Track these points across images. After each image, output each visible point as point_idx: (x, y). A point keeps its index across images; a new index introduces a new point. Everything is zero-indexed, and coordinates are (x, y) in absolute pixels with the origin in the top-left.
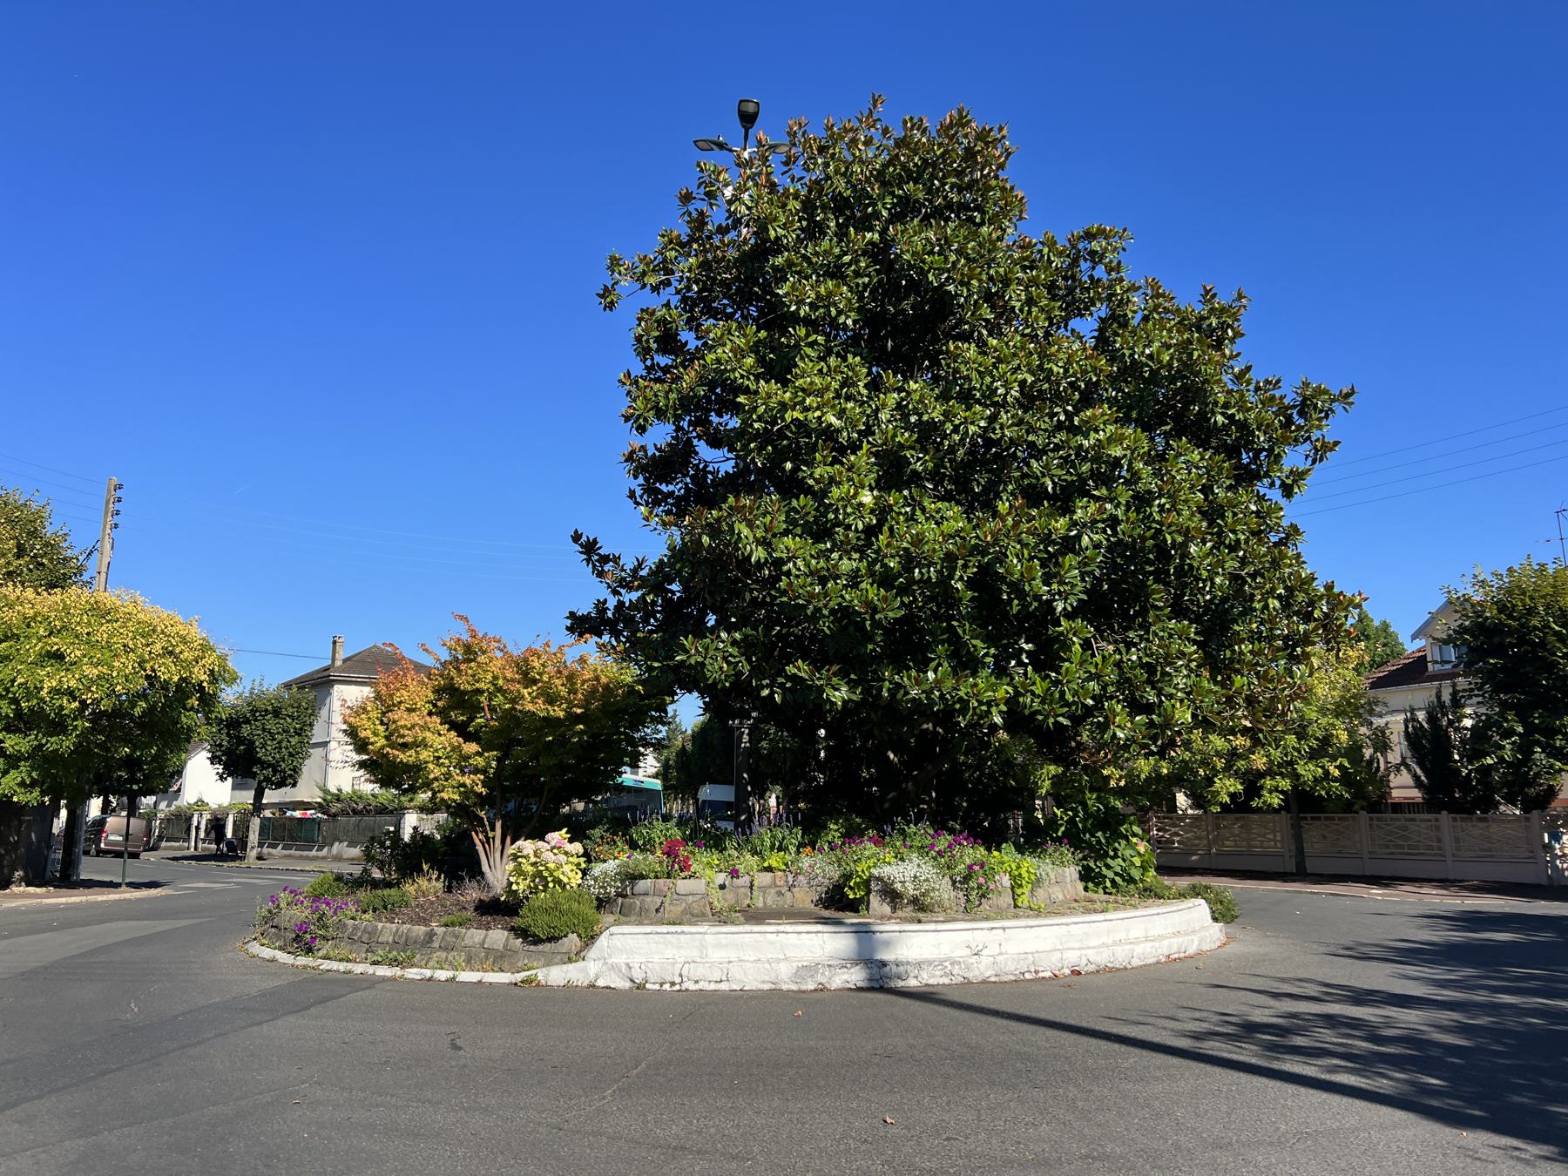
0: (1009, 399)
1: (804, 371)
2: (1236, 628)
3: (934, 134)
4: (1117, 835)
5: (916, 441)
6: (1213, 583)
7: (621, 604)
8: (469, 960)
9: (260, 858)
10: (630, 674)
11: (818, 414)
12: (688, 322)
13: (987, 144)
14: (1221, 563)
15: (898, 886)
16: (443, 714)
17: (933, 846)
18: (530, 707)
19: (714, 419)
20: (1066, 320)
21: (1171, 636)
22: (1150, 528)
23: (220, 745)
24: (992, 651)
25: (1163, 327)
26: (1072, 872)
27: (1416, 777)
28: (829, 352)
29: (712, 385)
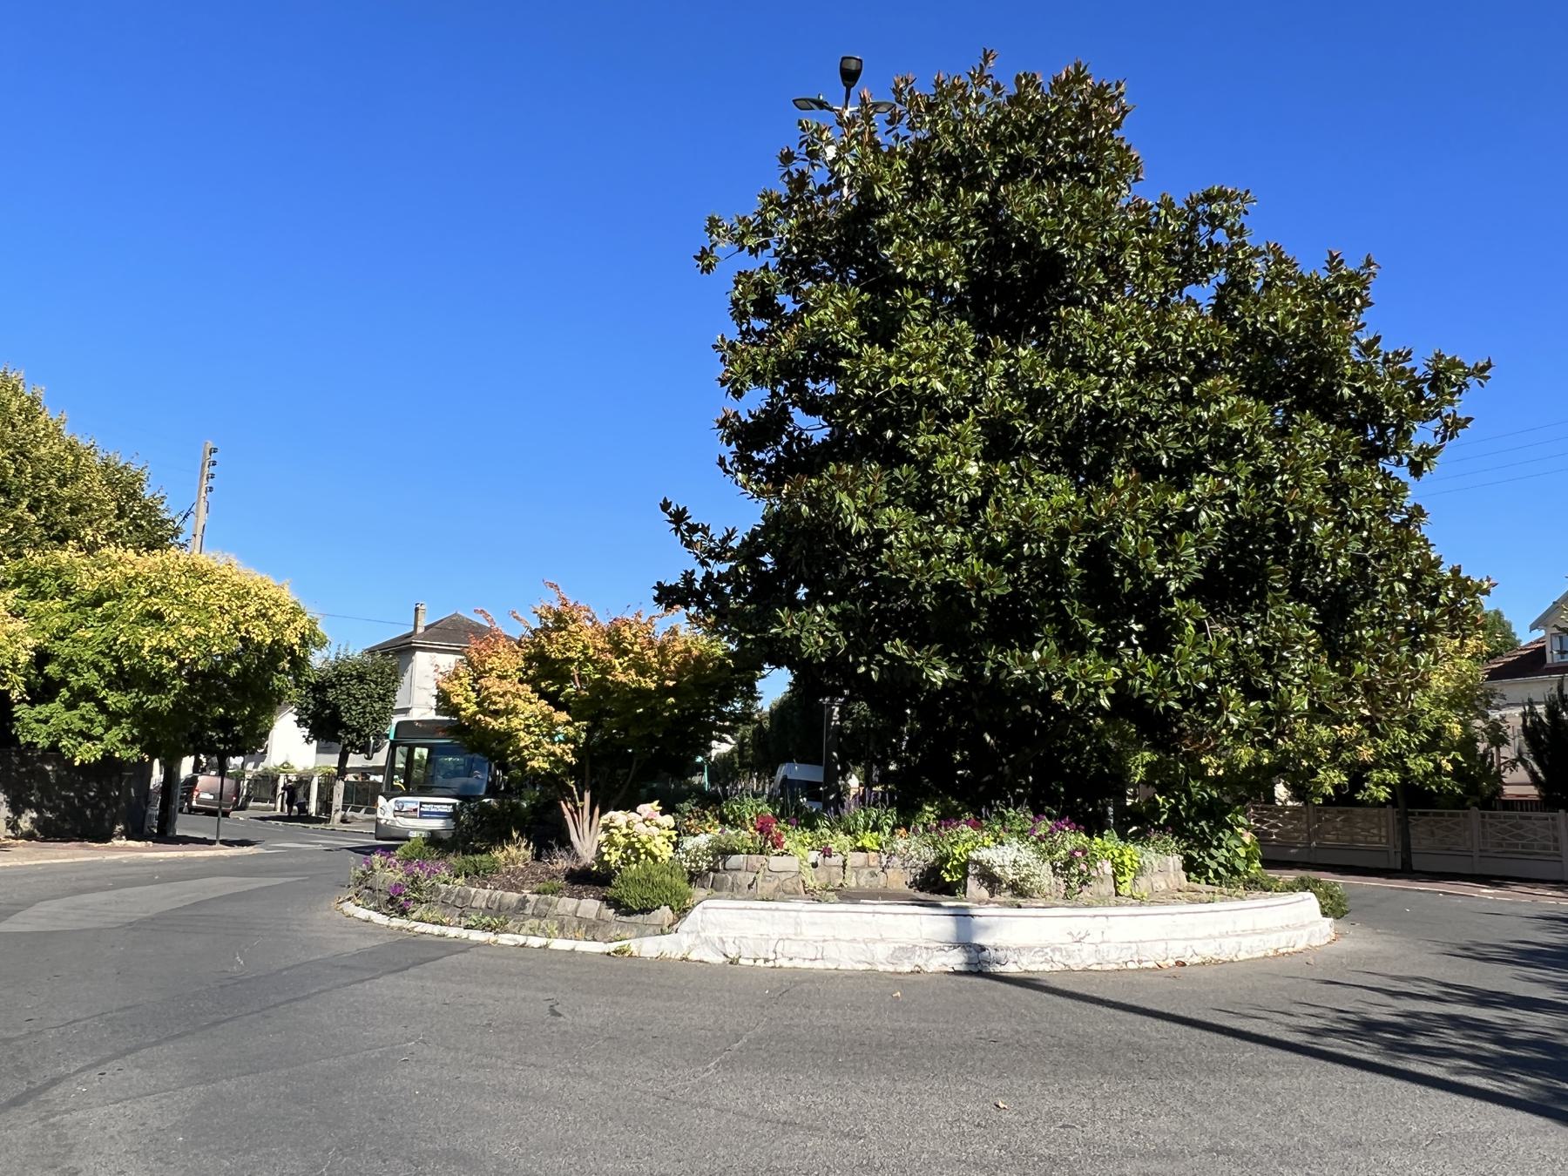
0: (1125, 368)
1: (909, 335)
2: (1357, 612)
3: (1047, 91)
4: (1221, 825)
5: (1027, 410)
6: (1335, 564)
7: (709, 575)
8: (561, 928)
9: (344, 821)
10: (723, 646)
11: (923, 379)
12: (786, 284)
13: (1104, 101)
14: (1344, 544)
15: (997, 870)
16: (533, 682)
17: (1033, 830)
18: (622, 678)
19: (810, 385)
20: (1181, 286)
21: (1288, 619)
22: (1270, 506)
23: (307, 709)
24: (1102, 631)
25: (1288, 295)
26: (1176, 861)
27: (1533, 774)
28: (935, 316)
29: (811, 349)
